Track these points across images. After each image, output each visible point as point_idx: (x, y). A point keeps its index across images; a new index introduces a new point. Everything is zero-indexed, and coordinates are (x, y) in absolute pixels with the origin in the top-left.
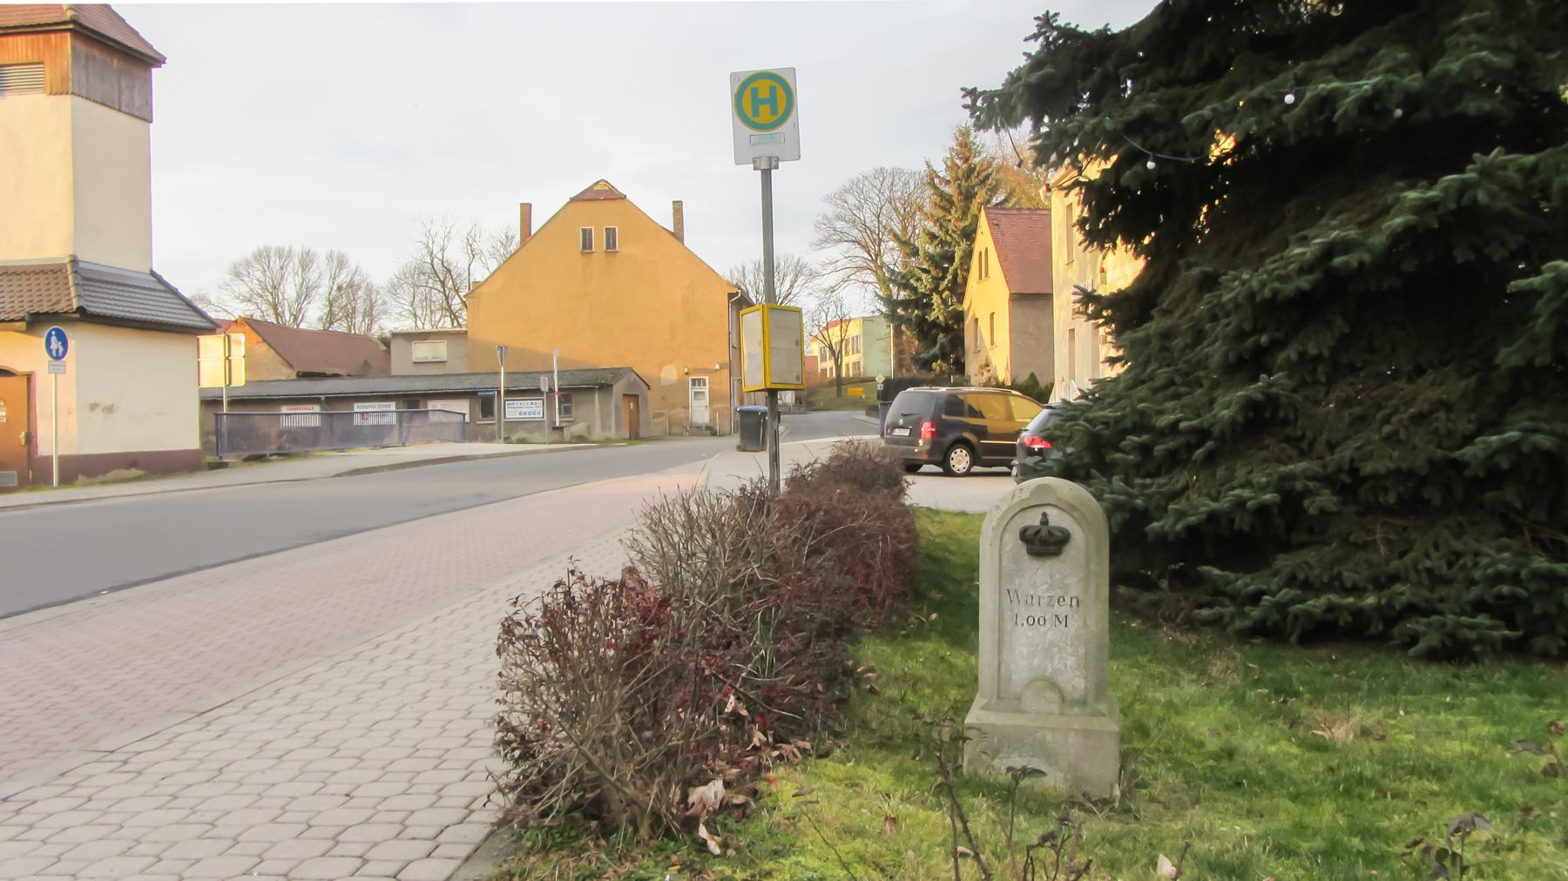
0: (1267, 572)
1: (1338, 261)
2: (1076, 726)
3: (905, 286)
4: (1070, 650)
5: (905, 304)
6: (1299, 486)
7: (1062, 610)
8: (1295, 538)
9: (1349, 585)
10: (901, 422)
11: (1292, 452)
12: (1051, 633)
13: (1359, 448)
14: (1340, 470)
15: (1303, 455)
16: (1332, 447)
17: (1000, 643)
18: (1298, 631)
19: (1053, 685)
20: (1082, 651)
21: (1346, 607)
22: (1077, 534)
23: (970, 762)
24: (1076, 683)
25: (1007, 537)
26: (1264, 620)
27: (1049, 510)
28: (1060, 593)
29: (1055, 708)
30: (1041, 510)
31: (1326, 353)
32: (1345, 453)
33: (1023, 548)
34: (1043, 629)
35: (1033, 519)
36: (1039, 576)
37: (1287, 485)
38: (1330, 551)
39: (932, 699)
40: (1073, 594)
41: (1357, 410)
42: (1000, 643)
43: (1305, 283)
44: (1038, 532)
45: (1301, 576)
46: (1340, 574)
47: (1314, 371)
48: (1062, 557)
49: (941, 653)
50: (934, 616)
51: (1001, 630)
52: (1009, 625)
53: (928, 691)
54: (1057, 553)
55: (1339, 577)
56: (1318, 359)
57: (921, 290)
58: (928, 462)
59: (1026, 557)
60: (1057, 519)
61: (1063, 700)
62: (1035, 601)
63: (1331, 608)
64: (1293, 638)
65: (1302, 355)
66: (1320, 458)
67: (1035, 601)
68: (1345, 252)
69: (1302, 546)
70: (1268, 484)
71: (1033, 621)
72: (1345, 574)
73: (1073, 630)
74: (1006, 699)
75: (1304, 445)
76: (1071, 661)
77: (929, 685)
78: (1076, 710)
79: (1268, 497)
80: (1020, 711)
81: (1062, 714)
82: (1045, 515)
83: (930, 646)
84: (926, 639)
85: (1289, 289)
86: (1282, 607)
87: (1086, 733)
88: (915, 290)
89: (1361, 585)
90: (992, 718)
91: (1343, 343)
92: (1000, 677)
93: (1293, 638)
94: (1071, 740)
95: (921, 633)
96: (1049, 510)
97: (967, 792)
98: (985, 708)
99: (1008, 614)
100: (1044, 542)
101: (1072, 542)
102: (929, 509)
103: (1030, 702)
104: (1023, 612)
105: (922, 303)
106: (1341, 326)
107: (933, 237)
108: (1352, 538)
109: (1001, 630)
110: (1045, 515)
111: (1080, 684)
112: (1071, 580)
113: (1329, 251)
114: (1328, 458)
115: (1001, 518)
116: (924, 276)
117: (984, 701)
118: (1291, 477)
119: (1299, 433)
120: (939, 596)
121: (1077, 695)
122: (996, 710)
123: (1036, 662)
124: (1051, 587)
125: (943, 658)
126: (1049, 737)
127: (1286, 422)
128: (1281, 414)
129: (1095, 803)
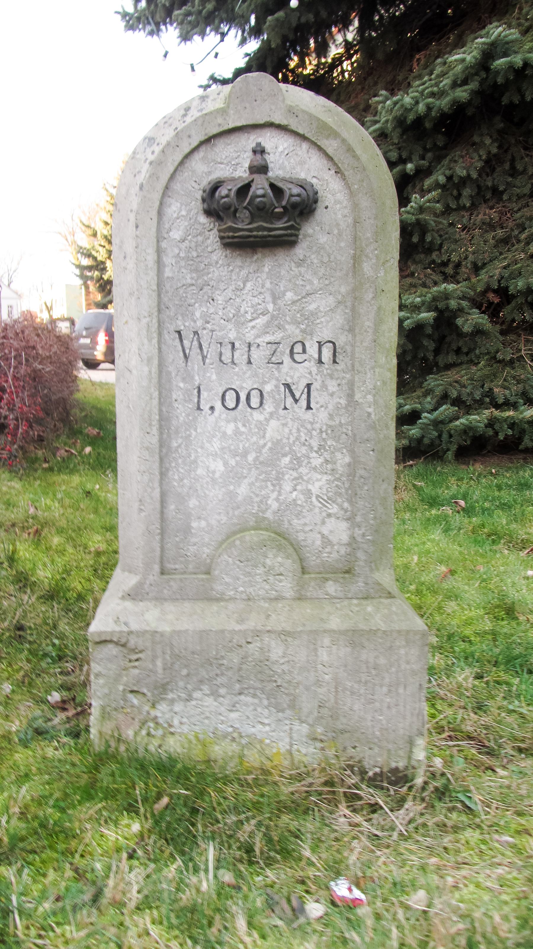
0: (419, 392)
1: (500, 62)
2: (335, 623)
3: (89, 255)
4: (317, 461)
5: (90, 268)
6: (453, 304)
7: (299, 374)
8: (442, 360)
9: (501, 401)
10: (84, 333)
11: (437, 277)
12: (275, 425)
13: (505, 268)
14: (488, 289)
15: (453, 278)
16: (477, 269)
17: (164, 455)
18: (454, 448)
19: (281, 538)
20: (343, 459)
21: (505, 420)
22: (332, 192)
23: (105, 715)
24: (328, 530)
25: (174, 208)
26: (420, 441)
27: (277, 146)
28: (294, 332)
29: (286, 587)
30: (250, 141)
31: (474, 175)
32: (495, 271)
33: (210, 234)
34: (257, 416)
35: (231, 163)
36: (250, 295)
37: (441, 305)
38: (480, 369)
39: (62, 552)
40: (326, 334)
41: (500, 233)
42: (164, 455)
43: (462, 94)
44: (244, 190)
45: (454, 394)
46: (491, 389)
47: (459, 196)
48: (299, 251)
49: (89, 487)
50: (88, 449)
51: (164, 421)
52: (181, 411)
53: (56, 540)
54: (286, 242)
55: (490, 393)
56: (464, 181)
57: (99, 258)
58: (104, 362)
59: (218, 255)
60: (290, 162)
61: (304, 571)
62: (240, 356)
63: (491, 423)
64: (450, 455)
65: (449, 178)
66: (468, 279)
67: (240, 356)
68: (505, 54)
69: (448, 367)
70: (423, 303)
71: (237, 401)
72: (496, 390)
73: (323, 416)
74: (177, 573)
75: (449, 270)
76: (319, 484)
77: (60, 531)
78: (331, 588)
79: (424, 315)
80: (208, 597)
81: (300, 598)
82: (259, 151)
83: (76, 479)
84: (72, 471)
85: (444, 103)
86: (437, 423)
87: (355, 638)
88: (95, 259)
89: (512, 399)
90: (151, 618)
91: (490, 165)
92: (165, 526)
93: (450, 455)
94: (324, 656)
95: (66, 466)
96: (271, 141)
97: (90, 809)
98: (133, 595)
99: (179, 388)
100: (261, 211)
101: (320, 213)
102: (101, 382)
103: (229, 576)
104: (213, 380)
105: (100, 266)
106: (489, 144)
107: (106, 224)
108: (500, 356)
109: (164, 421)
110: (259, 151)
111: (339, 531)
112: (320, 303)
113: (489, 54)
114: (474, 280)
115: (157, 164)
116: (100, 249)
117: (132, 580)
118: (446, 296)
119: (445, 258)
120: (95, 431)
121: (333, 556)
122: (160, 599)
123: (243, 490)
124: (275, 322)
125: (88, 493)
126: (276, 651)
127: (429, 250)
128: (428, 239)
129: (375, 782)
